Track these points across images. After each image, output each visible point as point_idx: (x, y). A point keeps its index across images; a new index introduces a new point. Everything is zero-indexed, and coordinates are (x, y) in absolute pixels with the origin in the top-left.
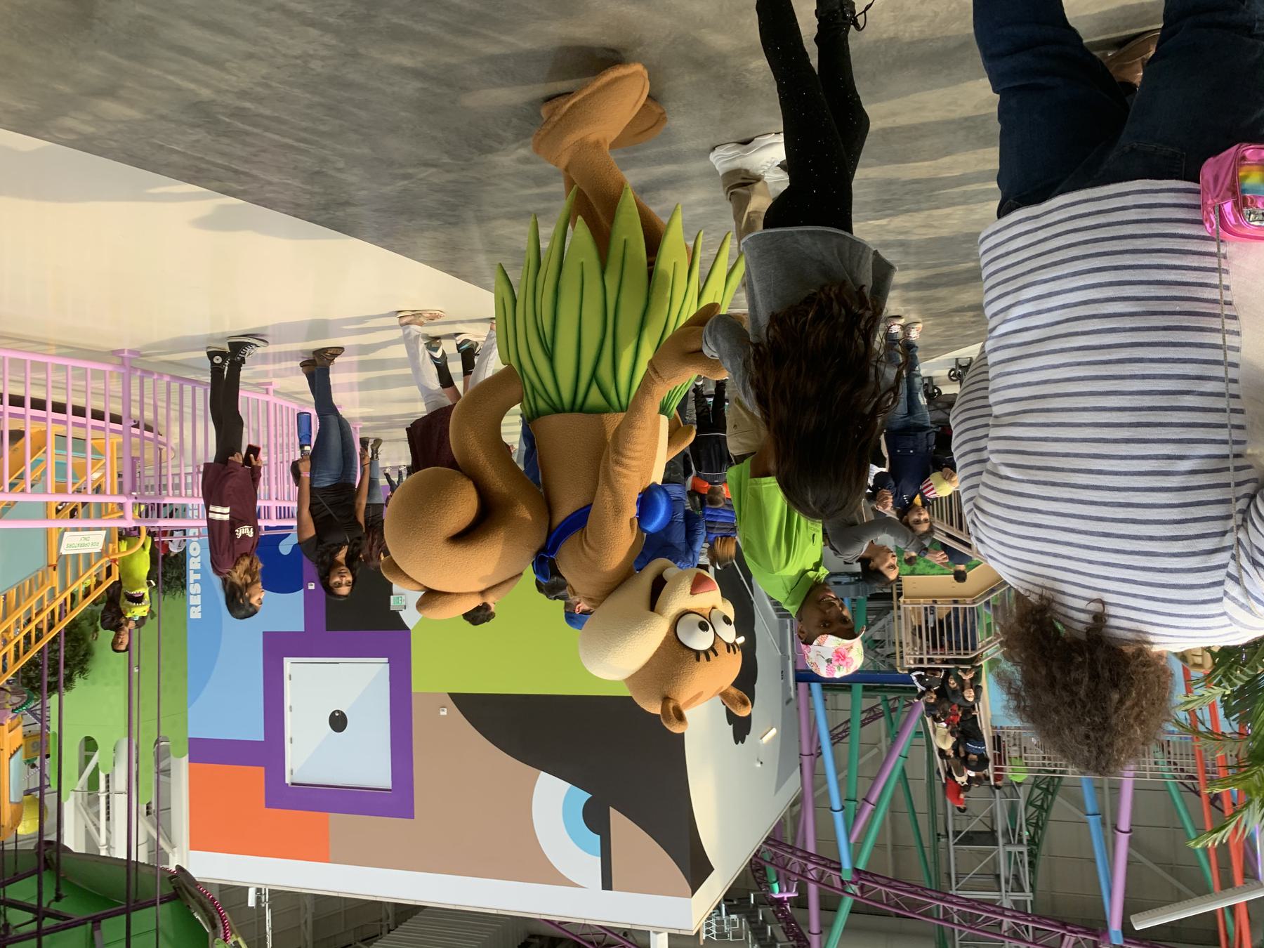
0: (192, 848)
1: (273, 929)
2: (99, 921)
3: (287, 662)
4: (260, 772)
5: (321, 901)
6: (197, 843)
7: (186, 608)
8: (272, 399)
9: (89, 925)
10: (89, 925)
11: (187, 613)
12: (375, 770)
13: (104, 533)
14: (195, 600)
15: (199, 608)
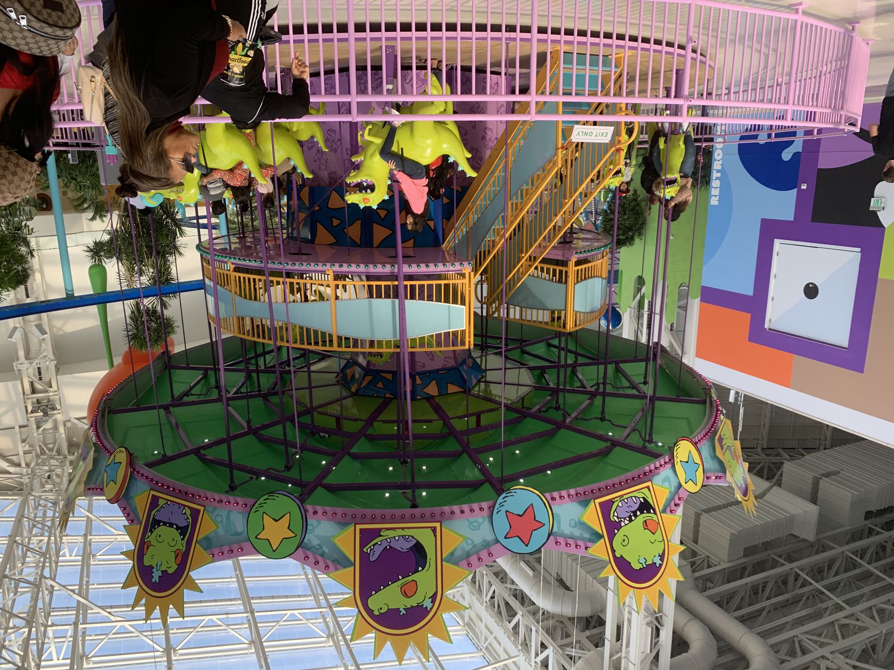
0: (697, 356)
1: (744, 419)
2: (616, 446)
3: (777, 243)
4: (748, 316)
5: (778, 412)
6: (699, 354)
7: (708, 197)
8: (800, 18)
10: (609, 444)
11: (709, 201)
12: (838, 333)
13: (612, 128)
14: (715, 192)
15: (717, 198)
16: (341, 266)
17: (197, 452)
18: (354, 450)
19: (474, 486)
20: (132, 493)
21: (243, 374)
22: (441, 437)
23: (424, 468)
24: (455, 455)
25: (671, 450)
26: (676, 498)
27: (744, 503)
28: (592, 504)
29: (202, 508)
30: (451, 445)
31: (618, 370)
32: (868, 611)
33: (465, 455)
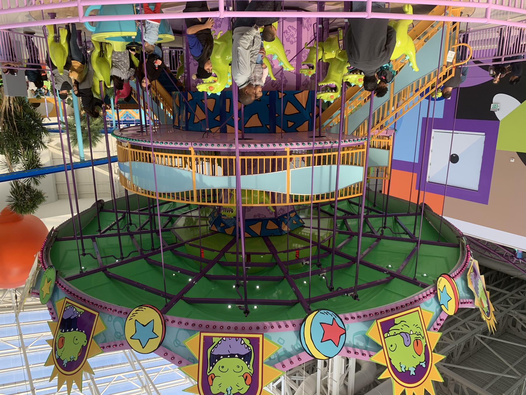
9: (394, 217)
12: (472, 182)
16: (213, 145)
17: (104, 269)
18: (211, 272)
19: (292, 304)
20: (56, 299)
21: (148, 216)
22: (271, 265)
23: (258, 287)
24: (279, 280)
25: (435, 283)
26: (438, 319)
27: (488, 322)
28: (375, 323)
29: (97, 314)
30: (277, 272)
31: (396, 221)
32: (517, 293)
33: (285, 280)
